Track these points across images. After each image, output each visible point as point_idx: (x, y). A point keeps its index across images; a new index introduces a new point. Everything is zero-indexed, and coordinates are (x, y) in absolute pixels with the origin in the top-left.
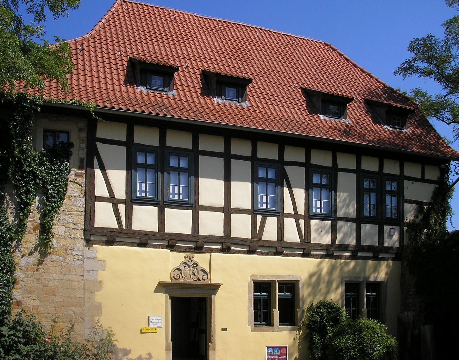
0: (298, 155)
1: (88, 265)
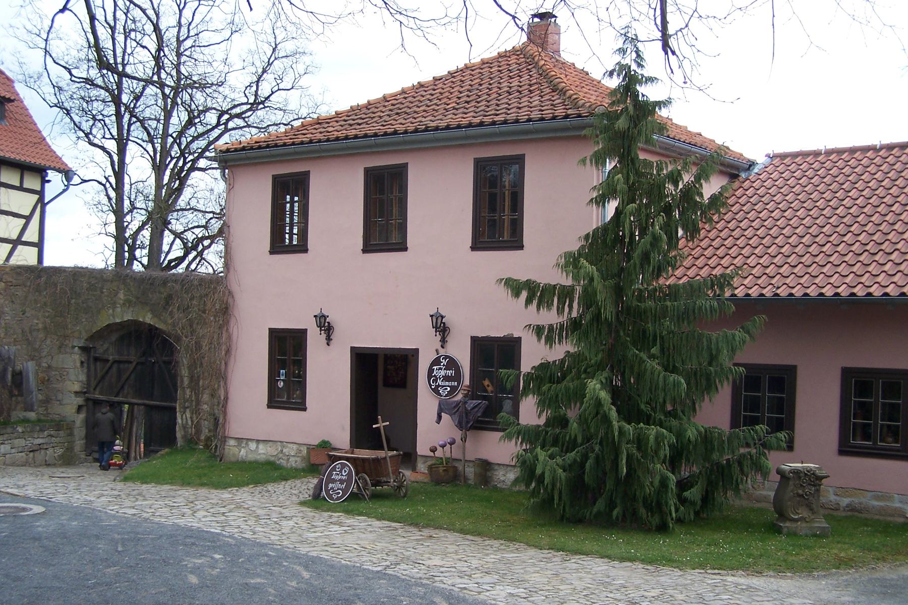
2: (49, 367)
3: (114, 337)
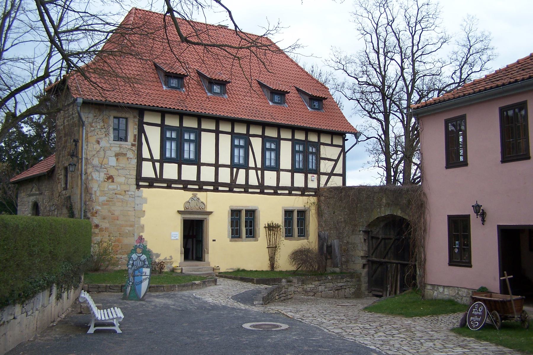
0: (258, 131)
1: (138, 201)
2: (348, 242)
3: (382, 224)
